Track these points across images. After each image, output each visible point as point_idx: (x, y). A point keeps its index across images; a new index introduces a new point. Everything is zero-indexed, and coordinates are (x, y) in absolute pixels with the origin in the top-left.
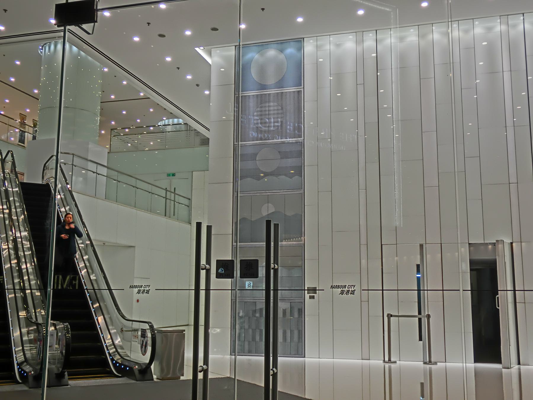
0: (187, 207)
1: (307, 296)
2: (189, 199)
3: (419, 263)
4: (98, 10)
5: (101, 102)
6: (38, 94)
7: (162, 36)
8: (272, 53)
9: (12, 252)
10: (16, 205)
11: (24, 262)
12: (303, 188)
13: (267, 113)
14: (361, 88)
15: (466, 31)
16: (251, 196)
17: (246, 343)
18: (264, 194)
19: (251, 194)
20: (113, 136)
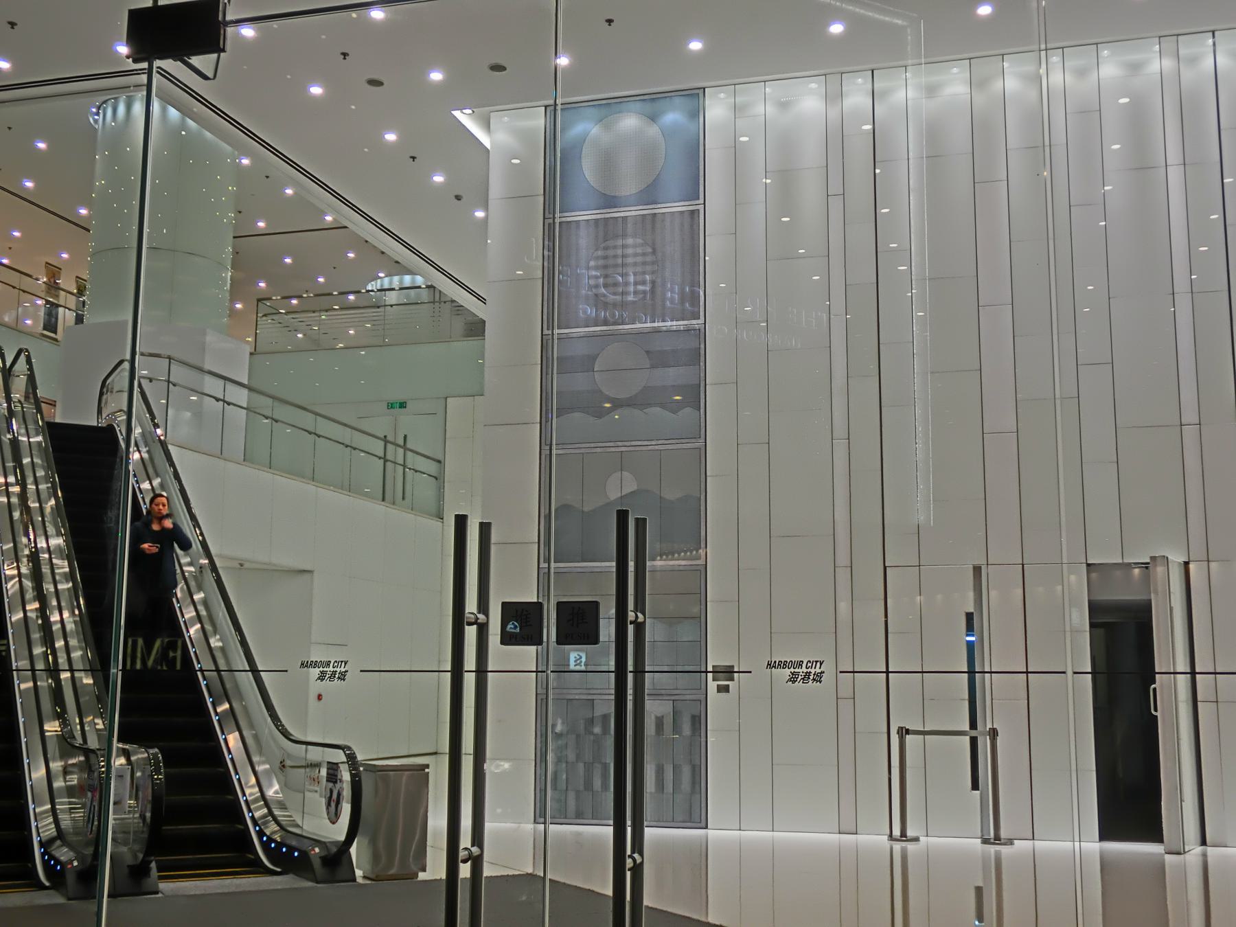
0: (435, 480)
1: (712, 686)
2: (439, 462)
3: (971, 610)
4: (226, 24)
5: (234, 237)
6: (89, 218)
7: (375, 83)
8: (630, 122)
9: (28, 584)
10: (38, 475)
12: (703, 436)
13: (620, 261)
14: (836, 204)
15: (1081, 73)
16: (583, 454)
17: (571, 796)
18: (613, 449)
19: (582, 451)
20: (263, 316)
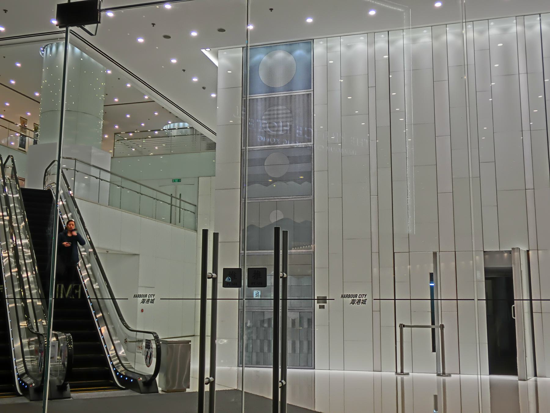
0: (193, 214)
1: (317, 305)
2: (195, 206)
3: (432, 272)
5: (104, 106)
6: (40, 97)
7: (167, 37)
8: (280, 54)
9: (12, 260)
10: (17, 212)
11: (25, 271)
12: (313, 194)
13: (276, 116)
14: (372, 91)
15: (481, 32)
16: (259, 202)
17: (254, 355)
18: (273, 200)
19: (259, 201)
20: (117, 141)
